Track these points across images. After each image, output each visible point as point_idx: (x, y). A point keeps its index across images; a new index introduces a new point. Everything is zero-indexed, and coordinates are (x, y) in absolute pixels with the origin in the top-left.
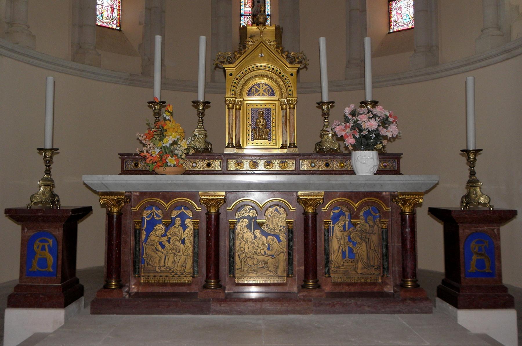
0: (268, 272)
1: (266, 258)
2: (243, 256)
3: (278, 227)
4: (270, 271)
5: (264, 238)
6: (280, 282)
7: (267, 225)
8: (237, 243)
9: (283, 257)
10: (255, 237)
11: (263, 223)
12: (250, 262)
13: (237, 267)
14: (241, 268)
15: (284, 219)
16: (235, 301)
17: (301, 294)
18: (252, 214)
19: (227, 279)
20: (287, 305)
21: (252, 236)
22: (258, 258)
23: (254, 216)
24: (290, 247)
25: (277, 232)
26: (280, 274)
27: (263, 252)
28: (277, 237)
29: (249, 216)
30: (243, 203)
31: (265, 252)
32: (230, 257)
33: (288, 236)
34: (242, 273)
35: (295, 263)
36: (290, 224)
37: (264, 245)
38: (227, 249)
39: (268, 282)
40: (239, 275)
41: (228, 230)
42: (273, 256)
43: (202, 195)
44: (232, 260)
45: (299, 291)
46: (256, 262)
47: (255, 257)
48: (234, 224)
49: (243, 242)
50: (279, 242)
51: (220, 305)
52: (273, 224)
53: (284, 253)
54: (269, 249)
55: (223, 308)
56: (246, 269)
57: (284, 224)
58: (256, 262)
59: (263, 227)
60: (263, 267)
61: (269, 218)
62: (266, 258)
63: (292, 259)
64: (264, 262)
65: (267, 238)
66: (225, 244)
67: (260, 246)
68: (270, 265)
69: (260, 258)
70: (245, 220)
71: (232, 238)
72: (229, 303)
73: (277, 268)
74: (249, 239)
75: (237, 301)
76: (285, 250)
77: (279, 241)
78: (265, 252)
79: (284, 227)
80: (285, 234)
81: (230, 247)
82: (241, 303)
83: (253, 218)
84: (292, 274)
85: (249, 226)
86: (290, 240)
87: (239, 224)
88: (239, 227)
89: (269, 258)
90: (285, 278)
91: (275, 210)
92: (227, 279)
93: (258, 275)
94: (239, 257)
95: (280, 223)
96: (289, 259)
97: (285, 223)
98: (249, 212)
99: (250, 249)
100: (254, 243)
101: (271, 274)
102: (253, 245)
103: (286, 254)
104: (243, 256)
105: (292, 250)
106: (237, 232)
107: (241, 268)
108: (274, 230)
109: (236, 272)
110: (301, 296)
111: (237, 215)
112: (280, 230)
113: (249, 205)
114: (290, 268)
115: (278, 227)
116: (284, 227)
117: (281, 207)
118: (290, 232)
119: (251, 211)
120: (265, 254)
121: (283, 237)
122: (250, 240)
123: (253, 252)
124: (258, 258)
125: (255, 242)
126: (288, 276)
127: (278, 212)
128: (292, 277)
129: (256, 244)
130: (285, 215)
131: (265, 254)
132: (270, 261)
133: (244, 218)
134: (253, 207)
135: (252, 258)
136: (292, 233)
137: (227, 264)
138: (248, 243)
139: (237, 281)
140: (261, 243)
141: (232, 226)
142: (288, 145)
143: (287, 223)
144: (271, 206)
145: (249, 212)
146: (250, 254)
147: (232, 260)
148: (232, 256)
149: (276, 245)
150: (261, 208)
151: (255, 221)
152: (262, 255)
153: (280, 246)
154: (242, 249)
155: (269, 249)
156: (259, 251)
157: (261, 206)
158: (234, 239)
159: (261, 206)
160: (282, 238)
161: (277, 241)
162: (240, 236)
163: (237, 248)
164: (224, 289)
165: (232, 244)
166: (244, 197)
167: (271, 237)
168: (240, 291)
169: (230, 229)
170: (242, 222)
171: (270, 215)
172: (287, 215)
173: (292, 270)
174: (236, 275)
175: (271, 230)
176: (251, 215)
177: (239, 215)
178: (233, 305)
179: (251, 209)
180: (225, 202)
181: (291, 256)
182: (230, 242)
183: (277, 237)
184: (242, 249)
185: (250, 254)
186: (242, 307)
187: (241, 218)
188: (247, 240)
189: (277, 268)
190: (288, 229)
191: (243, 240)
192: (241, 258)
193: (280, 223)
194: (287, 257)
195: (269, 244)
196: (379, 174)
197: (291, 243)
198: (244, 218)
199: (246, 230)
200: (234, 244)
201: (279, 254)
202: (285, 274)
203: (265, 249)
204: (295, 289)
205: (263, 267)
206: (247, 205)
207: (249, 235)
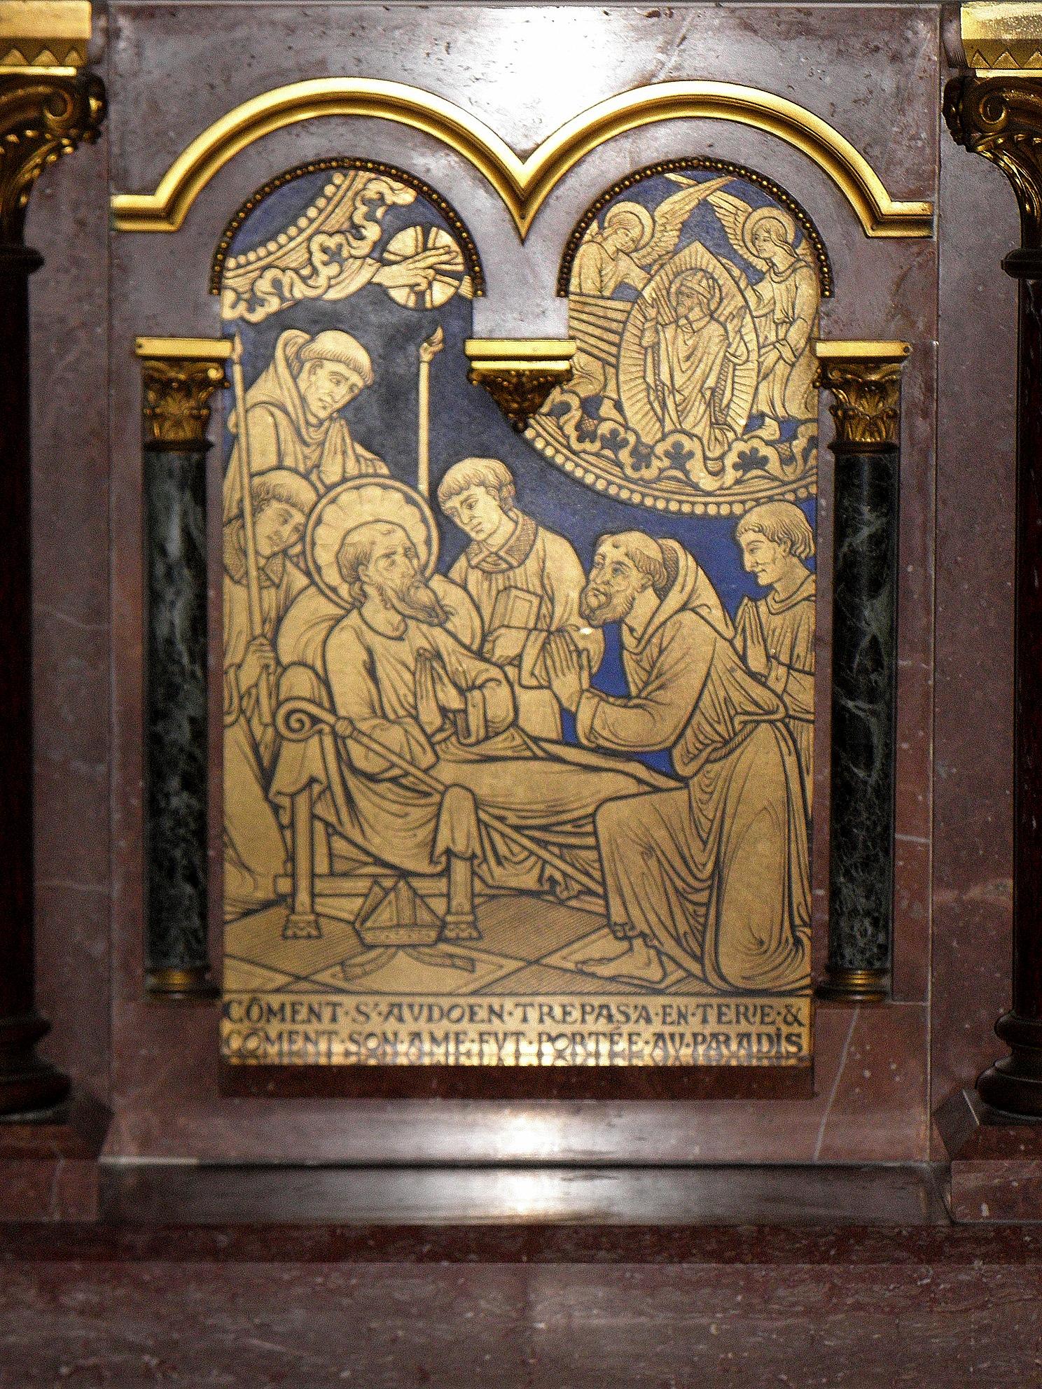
0: (603, 945)
1: (580, 790)
2: (307, 758)
3: (719, 422)
4: (625, 933)
5: (559, 555)
6: (734, 1054)
7: (590, 406)
8: (239, 608)
9: (773, 776)
10: (452, 541)
11: (545, 383)
12: (393, 833)
13: (236, 885)
14: (285, 900)
15: (796, 335)
16: (214, 1253)
17: (969, 1179)
18: (413, 271)
19: (124, 1016)
20: (814, 1293)
21: (416, 527)
22: (489, 781)
23: (440, 294)
24: (854, 661)
25: (709, 486)
26: (734, 967)
27: (539, 716)
28: (714, 544)
29: (376, 294)
30: (310, 146)
31: (568, 718)
32: (156, 770)
33: (843, 526)
34: (294, 957)
35: (914, 838)
36: (863, 389)
37: (550, 633)
38: (123, 682)
39: (596, 1053)
40: (259, 977)
41: (130, 460)
42: (658, 759)
43: (990, 49)
44: (179, 801)
45: (960, 1148)
46: (458, 831)
47: (447, 773)
48: (199, 385)
49: (312, 607)
50: (729, 606)
51: (51, 1290)
52: (659, 393)
53: (786, 724)
54: (609, 680)
55: (77, 1329)
56: (349, 907)
57: (792, 395)
58: (458, 831)
59: (540, 432)
60: (547, 891)
61: (609, 319)
62: (580, 790)
63: (885, 792)
64: (555, 829)
65: (587, 559)
66: (98, 612)
67: (506, 646)
68: (631, 870)
69: (513, 784)
70: (332, 342)
71: (175, 546)
72: (155, 1270)
73: (700, 894)
74: (375, 572)
75: (235, 1253)
76: (804, 693)
77: (736, 586)
78: (568, 718)
79: (789, 428)
80: (808, 506)
81: (158, 657)
82: (288, 1272)
83: (421, 321)
84: (880, 959)
85: (378, 421)
86: (857, 574)
87: (266, 388)
88: (260, 427)
89: (609, 783)
90: (803, 1007)
91: (688, 230)
92: (124, 1016)
93: (486, 970)
94: (266, 776)
95: (747, 376)
96: (842, 792)
97: (802, 378)
98: (379, 254)
99: (396, 681)
100: (438, 615)
101: (639, 963)
102: (419, 637)
103: (807, 737)
104: (307, 758)
105: (884, 696)
106: (231, 488)
107: (285, 900)
108: (679, 457)
109: (236, 938)
110: (972, 1199)
111: (235, 280)
112: (750, 462)
113: (383, 170)
114: (854, 895)
115: (719, 422)
116: (789, 428)
117: (756, 186)
118: (861, 480)
119: (406, 241)
120: (568, 736)
121: (777, 543)
122: (388, 575)
123: (430, 716)
124: (489, 781)
125: (452, 596)
126: (829, 988)
127: (719, 243)
128: (878, 996)
129: (465, 623)
130: (806, 289)
131: (568, 736)
132: (627, 816)
133: (318, 318)
134: (425, 191)
135: (417, 788)
136: (885, 496)
137: (127, 844)
138: (377, 614)
139: (236, 1039)
140: (522, 610)
141: (177, 407)
142: (879, 423)
143: (831, 374)
144: (643, 183)
145: (379, 254)
146: (394, 736)
147: (179, 801)
148: (176, 760)
149: (694, 636)
150: (522, 198)
151: (454, 362)
152: (535, 749)
153: (737, 651)
154: (300, 683)
155: (609, 680)
156: (498, 701)
157: (523, 173)
158: (197, 559)
159: (523, 173)
160: (764, 560)
161: (708, 596)
162: (268, 529)
163: (242, 665)
164: (95, 1126)
165: (176, 617)
166: (320, 70)
167: (635, 540)
168: (275, 1153)
169: (154, 447)
170: (296, 365)
171: (624, 291)
172: (826, 284)
173: (881, 921)
174: (234, 978)
175: (642, 456)
176: (398, 281)
177: (259, 281)
178: (195, 1294)
179: (399, 219)
180: (88, 128)
181: (865, 754)
182: (154, 599)
183: (714, 544)
184: (300, 683)
185: (394, 736)
186: (298, 1315)
187: (280, 321)
188: (354, 569)
189: (700, 894)
190: (841, 446)
191: (312, 573)
192: (284, 780)
193: (747, 376)
194: (817, 778)
195: (612, 631)
196: (666, 596)
197: (873, 616)
198: (318, 318)
199: (342, 456)
200: (202, 622)
201: (728, 745)
202: (801, 970)
203: (569, 684)
204: (910, 1134)
205: (547, 891)
206: (360, 164)
207: (375, 516)
